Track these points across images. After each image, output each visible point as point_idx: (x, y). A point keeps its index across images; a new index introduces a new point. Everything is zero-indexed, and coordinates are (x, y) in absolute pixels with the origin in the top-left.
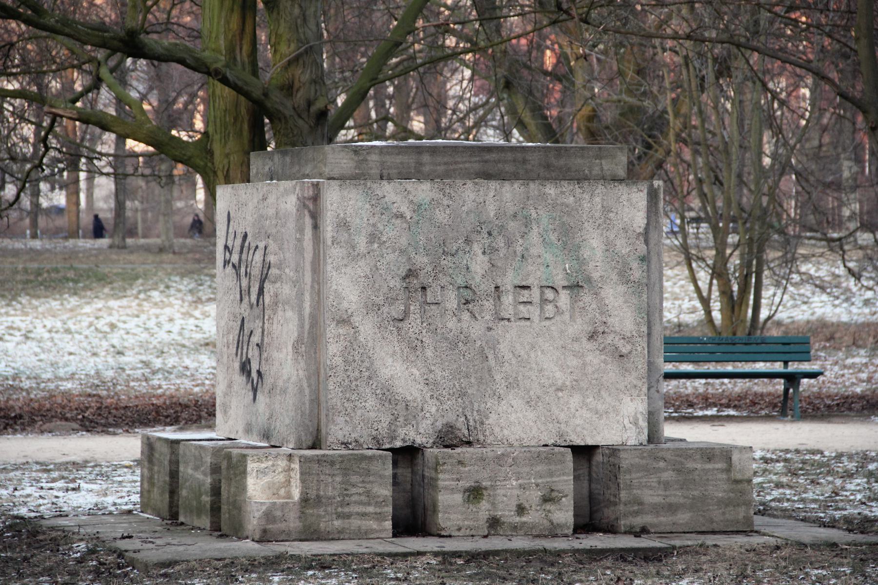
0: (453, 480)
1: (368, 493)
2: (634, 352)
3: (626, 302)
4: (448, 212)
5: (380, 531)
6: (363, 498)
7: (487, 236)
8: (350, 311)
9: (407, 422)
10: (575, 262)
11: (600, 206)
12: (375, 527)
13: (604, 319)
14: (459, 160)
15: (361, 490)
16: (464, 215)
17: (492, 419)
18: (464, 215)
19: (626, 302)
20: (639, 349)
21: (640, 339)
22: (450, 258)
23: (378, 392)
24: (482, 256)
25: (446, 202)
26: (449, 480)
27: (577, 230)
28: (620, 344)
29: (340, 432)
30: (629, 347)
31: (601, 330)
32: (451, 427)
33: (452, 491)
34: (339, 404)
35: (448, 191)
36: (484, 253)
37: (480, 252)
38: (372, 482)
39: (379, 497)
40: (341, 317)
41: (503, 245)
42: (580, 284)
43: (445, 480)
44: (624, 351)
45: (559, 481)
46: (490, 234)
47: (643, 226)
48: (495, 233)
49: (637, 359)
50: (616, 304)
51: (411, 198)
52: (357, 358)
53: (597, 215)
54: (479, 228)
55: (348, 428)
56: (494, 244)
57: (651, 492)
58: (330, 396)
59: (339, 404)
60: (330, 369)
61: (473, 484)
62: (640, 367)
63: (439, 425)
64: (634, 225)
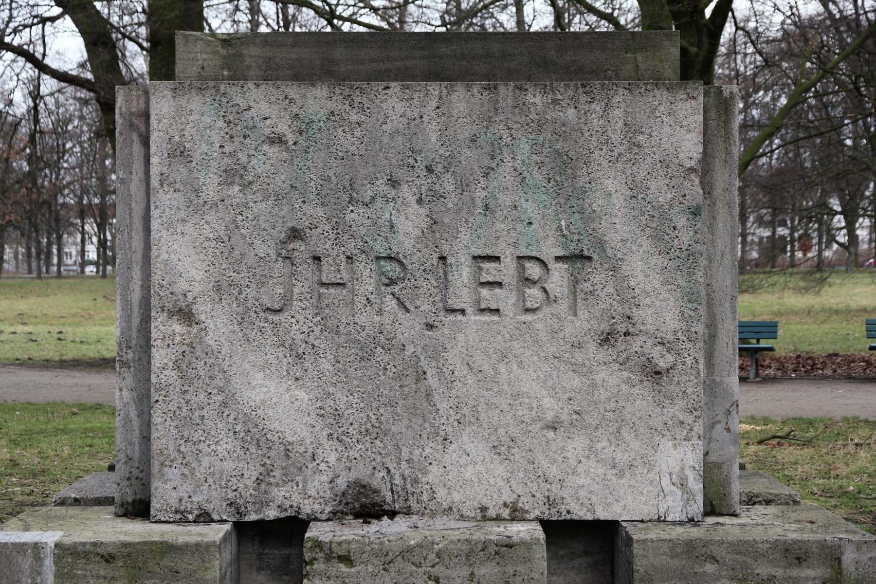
20: (689, 361)
44: (662, 364)
50: (649, 288)
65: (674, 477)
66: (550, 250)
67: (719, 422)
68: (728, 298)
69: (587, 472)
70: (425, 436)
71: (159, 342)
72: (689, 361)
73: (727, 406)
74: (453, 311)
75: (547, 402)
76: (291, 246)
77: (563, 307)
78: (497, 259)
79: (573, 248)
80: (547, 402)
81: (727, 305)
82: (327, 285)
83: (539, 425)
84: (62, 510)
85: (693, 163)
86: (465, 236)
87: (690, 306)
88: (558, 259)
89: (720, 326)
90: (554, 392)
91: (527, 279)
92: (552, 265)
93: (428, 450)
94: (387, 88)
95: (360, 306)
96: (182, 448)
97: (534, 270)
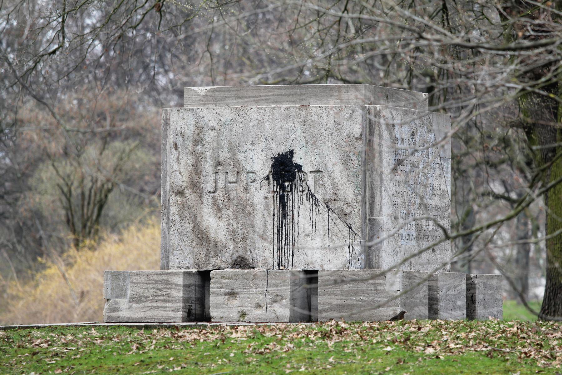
0: (218, 288)
1: (168, 295)
2: (353, 212)
3: (348, 181)
4: (241, 126)
5: (175, 318)
6: (165, 297)
7: (264, 140)
8: (183, 187)
9: (216, 255)
10: (317, 156)
11: (333, 121)
12: (172, 315)
13: (335, 192)
14: (262, 94)
15: (164, 293)
16: (251, 128)
17: (106, 244)
18: (251, 128)
19: (348, 181)
20: (356, 210)
21: (356, 204)
22: (242, 154)
23: (199, 236)
24: (261, 153)
25: (240, 120)
26: (215, 288)
27: (319, 136)
28: (345, 207)
29: (177, 260)
30: (350, 209)
31: (333, 198)
32: (243, 258)
33: (217, 294)
34: (176, 244)
35: (241, 113)
36: (263, 151)
37: (260, 151)
38: (171, 288)
39: (174, 297)
40: (178, 190)
41: (274, 146)
42: (320, 170)
43: (213, 288)
44: (347, 211)
45: (281, 290)
46: (266, 139)
47: (359, 133)
48: (269, 138)
49: (355, 217)
50: (343, 182)
51: (220, 118)
52: (187, 215)
53: (331, 127)
54: (260, 136)
55: (181, 258)
56: (268, 146)
57: (337, 297)
58: (171, 238)
59: (176, 244)
60: (172, 222)
61: (230, 291)
62: (357, 221)
63: (235, 257)
64: (354, 133)
72: (356, 210)
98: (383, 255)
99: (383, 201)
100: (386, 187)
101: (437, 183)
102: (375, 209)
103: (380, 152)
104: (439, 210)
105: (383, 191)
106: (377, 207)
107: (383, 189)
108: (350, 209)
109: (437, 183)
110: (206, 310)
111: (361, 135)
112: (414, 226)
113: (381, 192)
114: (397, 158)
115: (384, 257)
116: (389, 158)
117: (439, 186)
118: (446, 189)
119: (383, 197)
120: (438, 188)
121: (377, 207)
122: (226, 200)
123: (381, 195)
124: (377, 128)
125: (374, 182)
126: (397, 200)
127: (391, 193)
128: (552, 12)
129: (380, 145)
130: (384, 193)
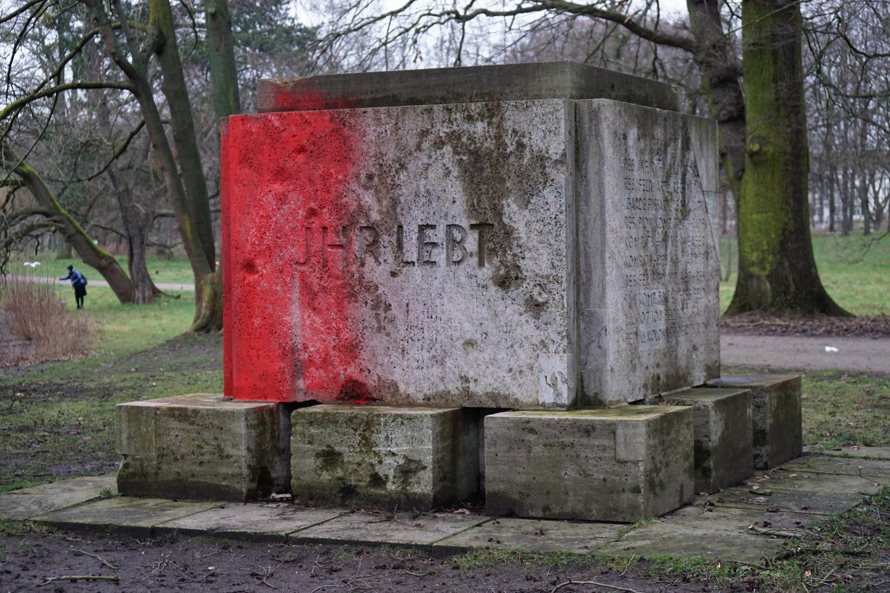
20: (557, 297)
44: (540, 300)
50: (530, 245)
65: (548, 379)
66: (465, 223)
67: (593, 341)
68: (599, 252)
69: (492, 374)
70: (391, 348)
71: (236, 284)
72: (557, 297)
73: (599, 330)
74: (408, 263)
75: (467, 326)
76: (311, 221)
77: (474, 260)
78: (433, 227)
79: (481, 219)
80: (467, 326)
81: (598, 257)
82: (340, 246)
83: (462, 341)
84: (286, 566)
85: (558, 157)
86: (416, 212)
87: (558, 258)
88: (472, 227)
89: (593, 272)
90: (471, 320)
91: (154, 292)
92: (468, 231)
93: (393, 358)
94: (365, 112)
95: (351, 260)
96: (250, 354)
97: (458, 236)
98: (609, 378)
99: (608, 278)
100: (612, 252)
101: (698, 234)
102: (592, 293)
103: (601, 186)
104: (702, 279)
105: (607, 260)
106: (596, 290)
107: (607, 255)
108: (545, 295)
109: (698, 234)
110: (481, 469)
111: (564, 155)
112: (663, 314)
113: (603, 263)
114: (632, 196)
115: (610, 383)
116: (617, 197)
117: (702, 239)
118: (712, 244)
119: (608, 270)
120: (701, 243)
121: (596, 290)
122: (325, 278)
123: (603, 268)
124: (593, 142)
125: (591, 243)
126: (633, 273)
127: (621, 262)
128: (772, 16)
129: (600, 173)
130: (608, 263)
